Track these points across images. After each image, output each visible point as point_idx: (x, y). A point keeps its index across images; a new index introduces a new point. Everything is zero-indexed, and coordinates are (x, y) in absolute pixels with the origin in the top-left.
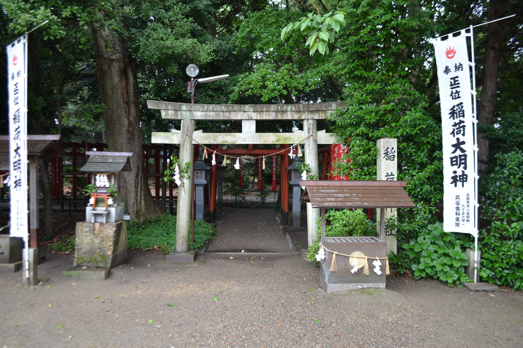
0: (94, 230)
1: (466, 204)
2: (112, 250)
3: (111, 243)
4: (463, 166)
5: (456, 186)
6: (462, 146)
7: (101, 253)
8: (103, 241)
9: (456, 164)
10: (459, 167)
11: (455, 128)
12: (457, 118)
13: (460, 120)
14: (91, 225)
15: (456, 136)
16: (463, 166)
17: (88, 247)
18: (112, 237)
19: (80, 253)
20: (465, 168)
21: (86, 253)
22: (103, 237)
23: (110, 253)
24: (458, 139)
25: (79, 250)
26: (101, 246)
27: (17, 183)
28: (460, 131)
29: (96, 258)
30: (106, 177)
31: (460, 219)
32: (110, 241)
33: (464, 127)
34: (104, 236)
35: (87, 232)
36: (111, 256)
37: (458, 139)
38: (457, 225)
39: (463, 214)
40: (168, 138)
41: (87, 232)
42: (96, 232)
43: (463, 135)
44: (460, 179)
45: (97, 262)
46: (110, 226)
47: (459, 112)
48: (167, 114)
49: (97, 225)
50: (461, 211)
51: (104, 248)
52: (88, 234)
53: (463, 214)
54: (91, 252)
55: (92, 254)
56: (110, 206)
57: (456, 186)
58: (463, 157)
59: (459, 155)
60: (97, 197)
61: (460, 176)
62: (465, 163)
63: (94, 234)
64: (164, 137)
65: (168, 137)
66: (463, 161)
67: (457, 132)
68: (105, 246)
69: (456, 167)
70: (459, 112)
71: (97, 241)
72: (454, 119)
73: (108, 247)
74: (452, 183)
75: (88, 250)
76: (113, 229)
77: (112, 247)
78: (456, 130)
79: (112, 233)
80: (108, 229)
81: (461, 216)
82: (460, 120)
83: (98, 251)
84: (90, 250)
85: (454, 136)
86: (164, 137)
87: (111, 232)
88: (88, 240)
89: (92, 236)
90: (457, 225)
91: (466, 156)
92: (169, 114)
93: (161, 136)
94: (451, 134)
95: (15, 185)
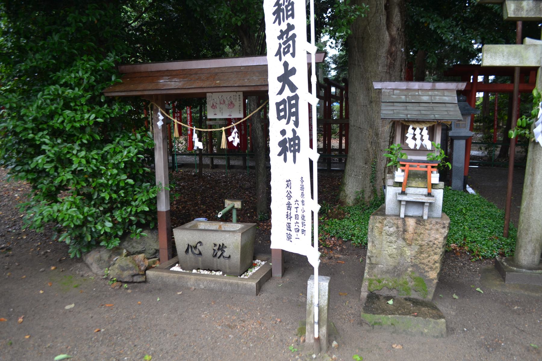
0: (405, 231)
1: (300, 199)
2: (438, 270)
3: (437, 257)
4: (293, 118)
5: (285, 160)
6: (292, 78)
7: (417, 275)
8: (421, 253)
9: (284, 117)
10: (288, 123)
11: (281, 41)
12: (284, 21)
13: (288, 24)
14: (400, 222)
15: (284, 59)
16: (293, 118)
17: (391, 262)
18: (440, 245)
19: (375, 270)
20: (296, 124)
21: (387, 272)
22: (421, 246)
23: (433, 275)
24: (286, 65)
25: (373, 266)
26: (417, 261)
27: (290, 146)
28: (289, 46)
29: (406, 283)
30: (425, 132)
31: (293, 227)
32: (435, 254)
33: (294, 36)
34: (424, 243)
35: (391, 235)
36: (436, 281)
37: (286, 65)
38: (289, 237)
39: (297, 217)
40: (516, 54)
41: (391, 235)
42: (407, 236)
43: (293, 55)
44: (291, 146)
45: (408, 290)
46: (437, 226)
47: (287, 7)
48: (519, 8)
49: (411, 223)
50: (293, 212)
51: (422, 266)
52: (393, 239)
53: (297, 217)
54: (396, 271)
55: (399, 275)
56: (434, 186)
57: (285, 160)
58: (293, 102)
59: (288, 97)
60: (411, 169)
61: (291, 140)
62: (296, 114)
63: (404, 239)
64: (509, 54)
65: (516, 53)
66: (293, 110)
67: (284, 49)
68: (425, 261)
69: (284, 121)
70: (287, 7)
71: (409, 252)
72: (280, 24)
73: (430, 264)
74: (280, 155)
75: (391, 268)
76: (443, 231)
77: (438, 265)
78: (283, 46)
79: (441, 239)
80: (433, 232)
81: (293, 221)
82: (288, 24)
83: (410, 269)
84: (395, 267)
85: (280, 59)
86: (509, 54)
87: (438, 236)
88: (392, 249)
89: (401, 242)
90: (289, 237)
91: (296, 97)
92: (522, 9)
93: (502, 52)
94: (276, 55)
95: (280, 149)
